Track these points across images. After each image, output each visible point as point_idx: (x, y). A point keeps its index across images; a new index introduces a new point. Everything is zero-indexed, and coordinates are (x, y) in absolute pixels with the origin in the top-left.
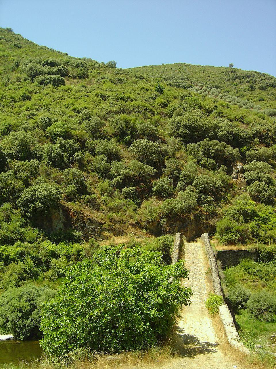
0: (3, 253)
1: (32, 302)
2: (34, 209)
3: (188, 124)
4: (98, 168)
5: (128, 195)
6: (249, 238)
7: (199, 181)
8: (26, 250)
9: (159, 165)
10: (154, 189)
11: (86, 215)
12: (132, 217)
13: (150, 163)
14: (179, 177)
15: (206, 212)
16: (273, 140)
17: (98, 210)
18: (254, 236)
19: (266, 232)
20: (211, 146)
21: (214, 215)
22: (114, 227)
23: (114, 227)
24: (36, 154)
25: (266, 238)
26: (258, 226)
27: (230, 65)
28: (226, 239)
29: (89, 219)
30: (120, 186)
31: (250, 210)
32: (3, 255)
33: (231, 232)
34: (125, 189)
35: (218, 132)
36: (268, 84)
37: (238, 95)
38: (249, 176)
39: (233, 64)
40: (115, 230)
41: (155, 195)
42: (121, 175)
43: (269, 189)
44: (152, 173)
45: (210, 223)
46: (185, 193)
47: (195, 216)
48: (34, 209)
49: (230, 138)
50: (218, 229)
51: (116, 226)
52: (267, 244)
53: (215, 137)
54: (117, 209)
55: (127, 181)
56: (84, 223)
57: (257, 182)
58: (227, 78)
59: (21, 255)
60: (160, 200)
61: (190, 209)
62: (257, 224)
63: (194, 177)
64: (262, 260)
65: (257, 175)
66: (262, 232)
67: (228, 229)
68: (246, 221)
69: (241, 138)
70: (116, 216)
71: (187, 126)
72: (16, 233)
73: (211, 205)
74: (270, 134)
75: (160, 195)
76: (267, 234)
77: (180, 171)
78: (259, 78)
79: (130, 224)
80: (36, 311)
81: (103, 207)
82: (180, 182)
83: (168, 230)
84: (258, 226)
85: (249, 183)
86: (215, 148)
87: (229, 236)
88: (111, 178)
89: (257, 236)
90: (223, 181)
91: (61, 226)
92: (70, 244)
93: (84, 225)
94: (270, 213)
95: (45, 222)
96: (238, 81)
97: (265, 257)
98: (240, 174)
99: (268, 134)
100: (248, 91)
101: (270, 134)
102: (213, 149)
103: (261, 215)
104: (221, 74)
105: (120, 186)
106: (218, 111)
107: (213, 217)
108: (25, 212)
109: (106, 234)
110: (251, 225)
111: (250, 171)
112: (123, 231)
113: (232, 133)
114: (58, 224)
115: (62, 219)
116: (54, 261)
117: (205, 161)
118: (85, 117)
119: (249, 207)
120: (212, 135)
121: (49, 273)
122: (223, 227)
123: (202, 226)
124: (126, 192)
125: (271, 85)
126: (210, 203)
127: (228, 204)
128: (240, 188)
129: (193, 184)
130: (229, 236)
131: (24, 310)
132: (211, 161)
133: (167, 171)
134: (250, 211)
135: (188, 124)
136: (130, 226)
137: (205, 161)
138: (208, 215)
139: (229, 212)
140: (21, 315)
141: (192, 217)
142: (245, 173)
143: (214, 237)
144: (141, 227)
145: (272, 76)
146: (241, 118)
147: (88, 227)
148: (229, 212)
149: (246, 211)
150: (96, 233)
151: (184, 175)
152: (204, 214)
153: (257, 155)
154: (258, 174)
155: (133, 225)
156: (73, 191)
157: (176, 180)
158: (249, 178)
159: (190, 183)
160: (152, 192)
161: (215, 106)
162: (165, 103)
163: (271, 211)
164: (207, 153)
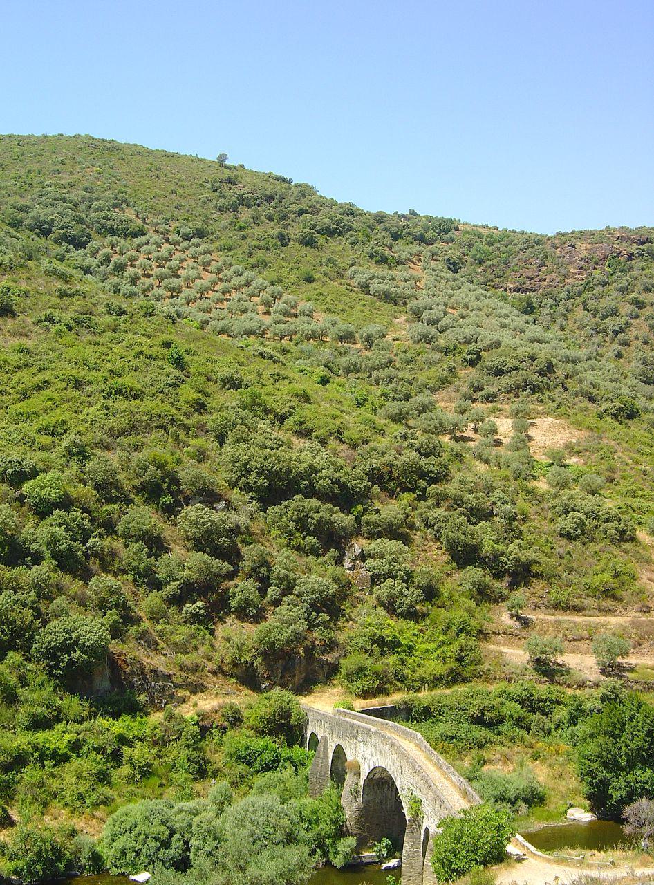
0: (47, 745)
1: (168, 824)
2: (71, 663)
3: (265, 468)
4: (135, 568)
5: (195, 618)
6: (391, 683)
7: (306, 588)
8: (80, 737)
9: (231, 555)
10: (233, 603)
11: (147, 664)
12: (210, 659)
13: (219, 553)
14: (268, 578)
15: (320, 640)
16: (400, 485)
17: (156, 650)
18: (398, 680)
19: (414, 672)
20: (309, 511)
21: (333, 645)
22: (189, 680)
23: (189, 680)
24: (28, 548)
25: (416, 681)
26: (403, 661)
27: (220, 157)
28: (359, 688)
29: (153, 671)
30: (177, 600)
31: (389, 636)
32: (48, 749)
33: (365, 675)
34: (188, 607)
35: (315, 481)
36: (318, 228)
37: (253, 260)
38: (374, 568)
39: (226, 155)
40: (190, 684)
41: (233, 612)
42: (178, 580)
43: (409, 593)
44: (223, 571)
45: (327, 660)
46: (283, 609)
47: (306, 650)
48: (71, 663)
49: (336, 491)
50: (343, 671)
51: (192, 678)
52: (418, 690)
53: (311, 492)
54: (183, 648)
55: (188, 591)
56: (145, 678)
57: (389, 581)
58: (221, 202)
59: (76, 746)
60: (243, 622)
61: (298, 638)
62: (401, 659)
63: (295, 579)
64: (416, 719)
65: (387, 566)
66: (410, 671)
67: (360, 672)
68: (383, 653)
69: (352, 490)
70: (187, 659)
71: (264, 470)
72: (48, 708)
73: (327, 629)
74: (395, 474)
75: (243, 613)
76: (417, 675)
77: (269, 567)
78: (294, 205)
79: (209, 671)
80: (177, 836)
81: (162, 644)
82: (273, 588)
83: (266, 676)
84: (403, 661)
85: (375, 580)
86: (317, 516)
87: (363, 683)
88: (158, 585)
89: (402, 679)
90: (336, 579)
91: (107, 684)
92: (138, 718)
93: (145, 681)
94: (414, 635)
95: (80, 682)
96: (245, 215)
97: (420, 714)
98: (358, 562)
99: (391, 472)
100: (275, 249)
101: (395, 474)
102: (313, 519)
103: (404, 642)
104: (201, 184)
105: (177, 600)
106: (296, 418)
107: (332, 649)
108: (52, 668)
109: (181, 693)
110: (391, 660)
111: (373, 557)
112: (202, 685)
113: (336, 482)
114: (102, 682)
115: (108, 672)
116: (127, 751)
117: (298, 539)
118: (75, 450)
119: (387, 632)
120: (307, 487)
121: (126, 770)
122: (353, 668)
123: (316, 664)
124: (191, 613)
125: (323, 229)
126: (326, 625)
127: (349, 622)
128: (360, 588)
129: (295, 592)
130: (363, 683)
131: (163, 838)
132: (311, 540)
133: (246, 565)
134: (390, 638)
135: (265, 468)
136: (209, 674)
137: (298, 539)
138: (323, 645)
139: (356, 640)
140: (158, 844)
141: (301, 650)
142: (367, 561)
143: (335, 682)
144: (225, 674)
145: (321, 197)
146: (339, 431)
147: (153, 684)
148: (356, 640)
149: (383, 638)
150: (167, 693)
151: (278, 575)
152: (318, 645)
153: (381, 524)
154: (390, 564)
155: (214, 673)
156: (115, 621)
157: (265, 583)
158: (375, 571)
159: (288, 590)
160: (230, 607)
161: (290, 407)
162: (200, 400)
163: (415, 632)
164: (302, 524)
